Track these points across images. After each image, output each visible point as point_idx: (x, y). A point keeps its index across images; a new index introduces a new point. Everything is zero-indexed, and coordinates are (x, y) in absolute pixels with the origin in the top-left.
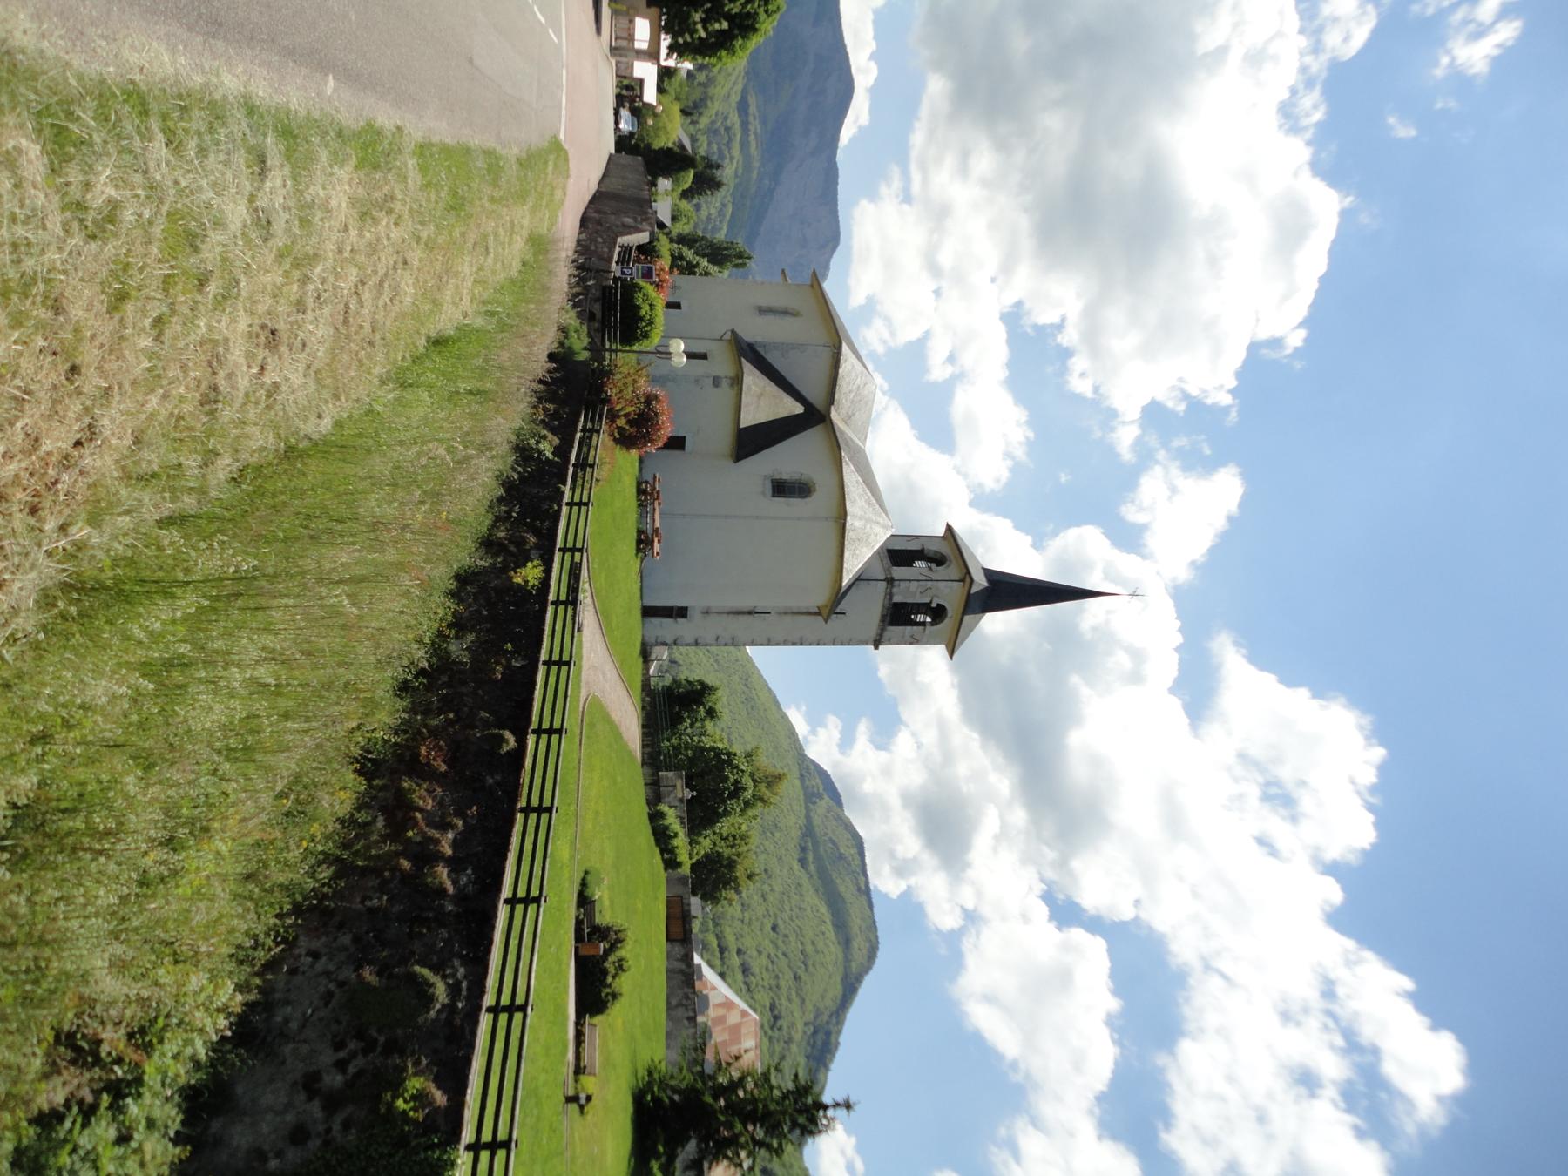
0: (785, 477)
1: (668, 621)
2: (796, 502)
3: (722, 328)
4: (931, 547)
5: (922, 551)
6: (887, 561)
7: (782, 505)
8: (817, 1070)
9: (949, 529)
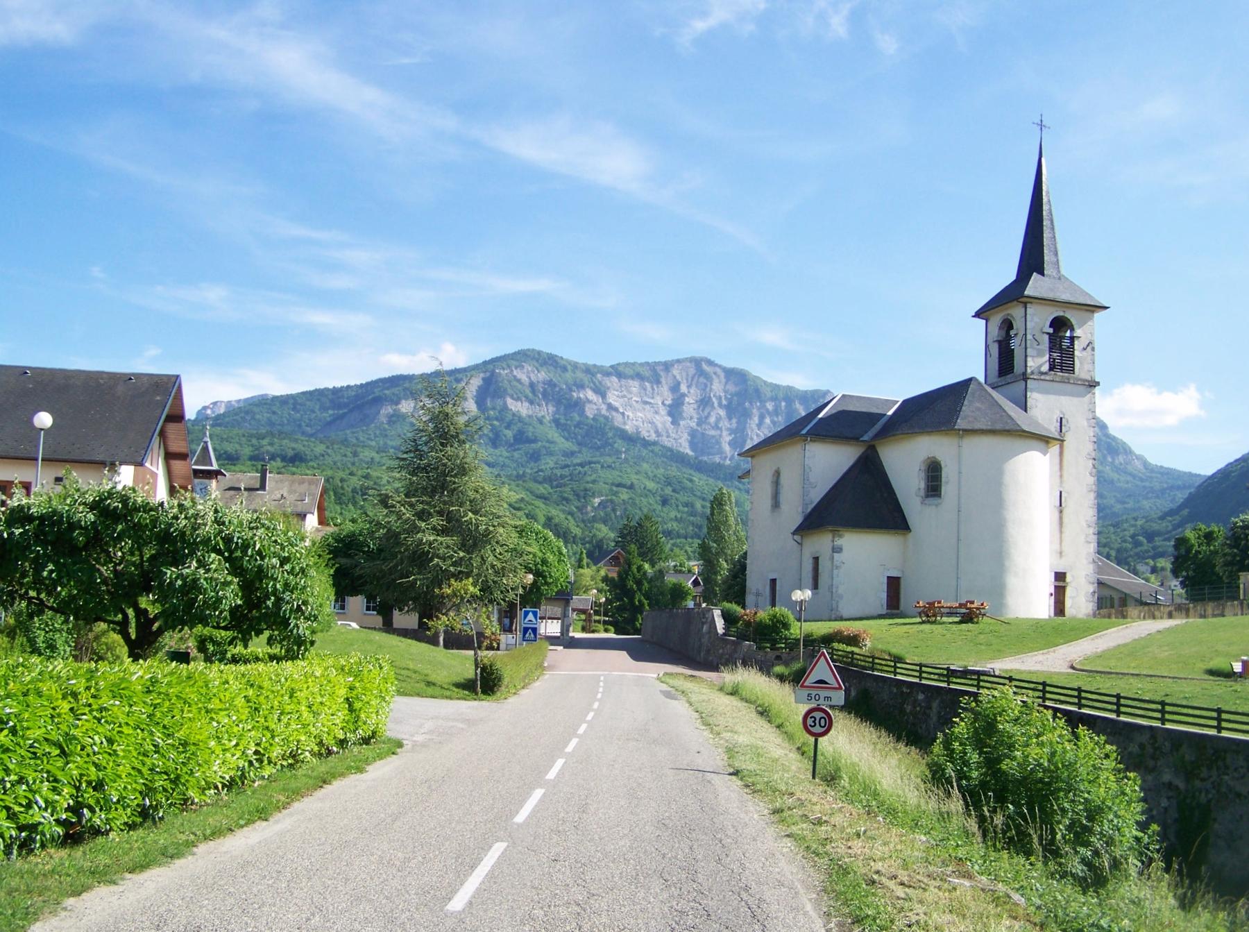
0: (923, 485)
1: (1069, 592)
2: (948, 473)
3: (790, 542)
4: (995, 332)
5: (999, 342)
6: (1009, 378)
7: (947, 489)
8: (815, 640)
9: (978, 315)
